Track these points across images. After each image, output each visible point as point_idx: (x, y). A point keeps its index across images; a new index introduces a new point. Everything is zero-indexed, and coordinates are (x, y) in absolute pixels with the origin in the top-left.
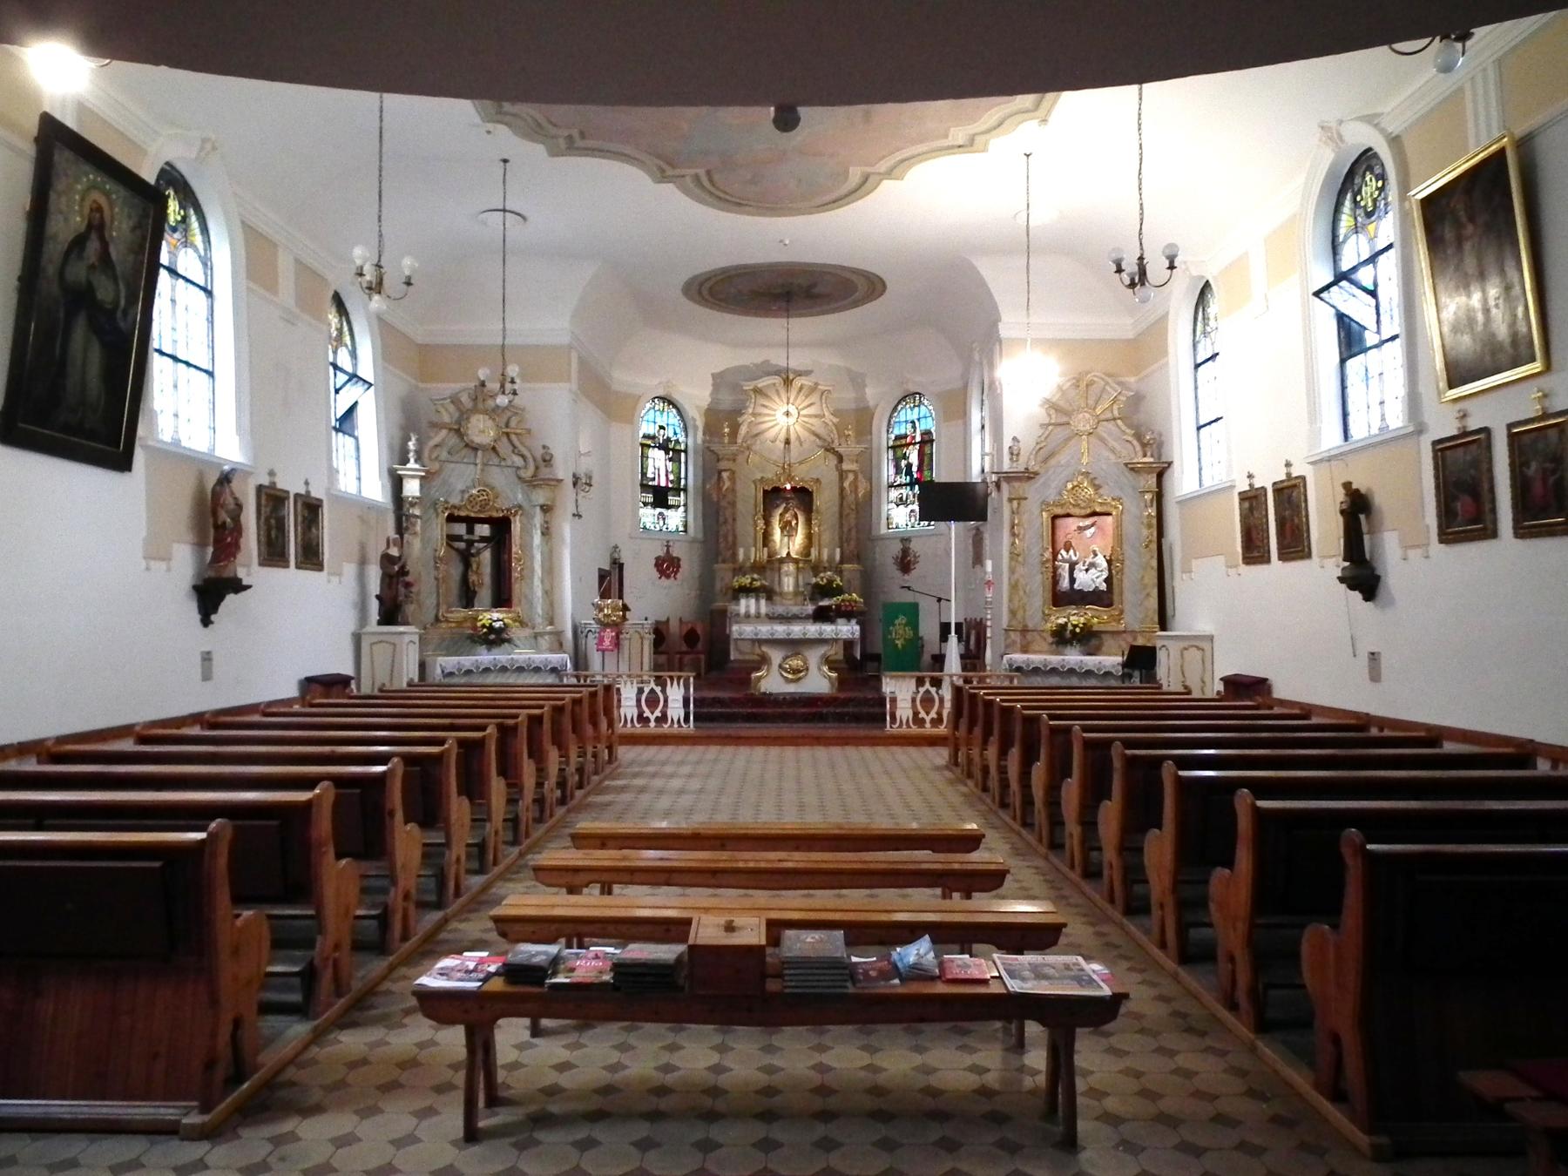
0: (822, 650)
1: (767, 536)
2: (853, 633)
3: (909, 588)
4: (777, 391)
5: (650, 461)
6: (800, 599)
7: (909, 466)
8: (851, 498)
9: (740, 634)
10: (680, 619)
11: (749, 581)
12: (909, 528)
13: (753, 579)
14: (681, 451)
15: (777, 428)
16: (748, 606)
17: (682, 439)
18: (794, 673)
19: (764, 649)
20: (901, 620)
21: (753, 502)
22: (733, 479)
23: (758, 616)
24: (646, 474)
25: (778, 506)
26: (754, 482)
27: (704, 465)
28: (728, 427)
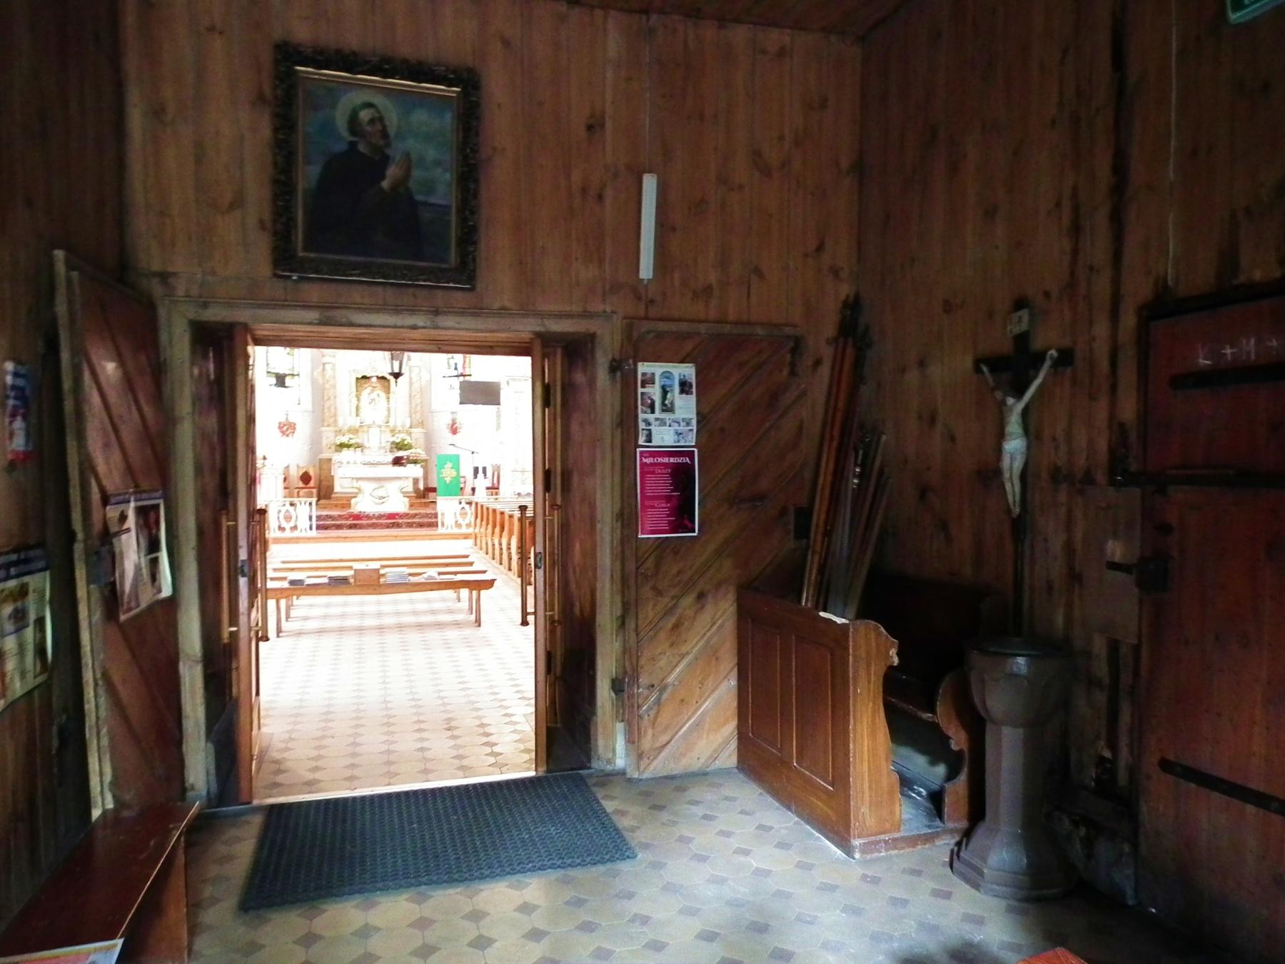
3: (453, 445)
6: (383, 451)
8: (416, 385)
10: (298, 466)
11: (348, 439)
20: (449, 465)
22: (333, 369)
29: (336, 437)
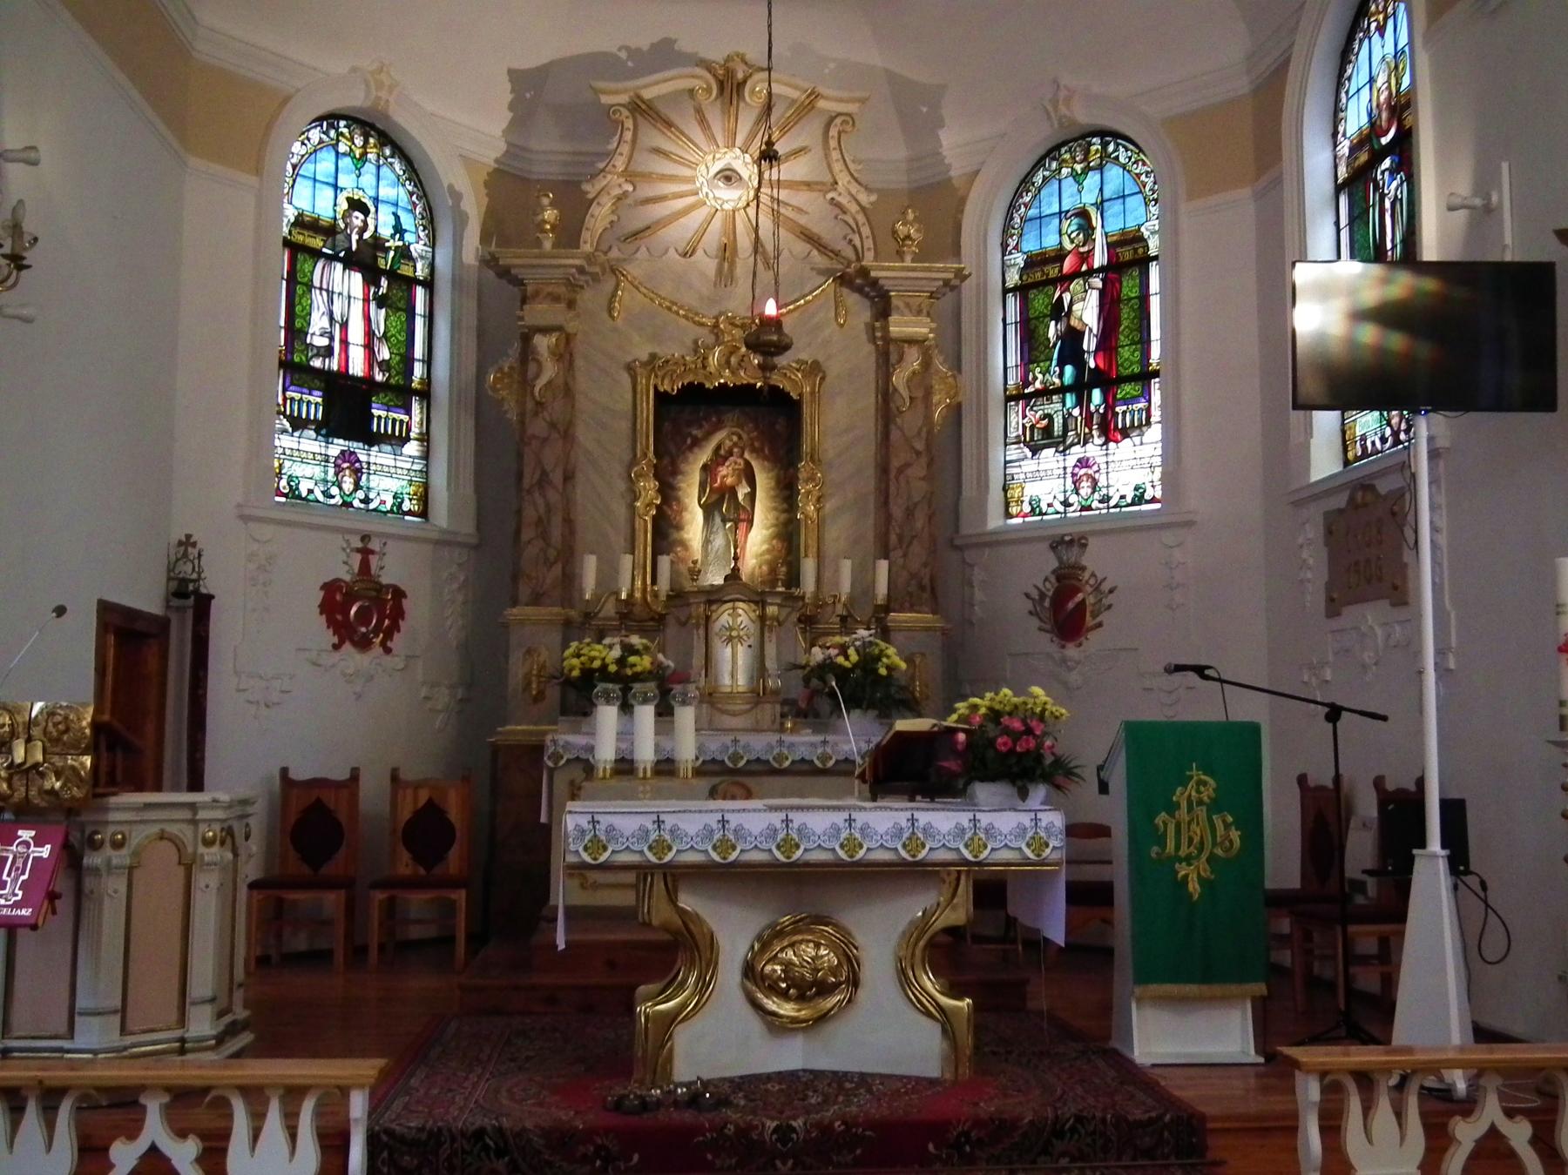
0: (913, 906)
1: (665, 530)
2: (1039, 844)
3: (1200, 671)
4: (699, 111)
5: (319, 299)
6: (769, 711)
7: (1072, 338)
8: (909, 421)
9: (597, 845)
10: (395, 777)
11: (616, 652)
12: (1073, 513)
13: (629, 650)
14: (415, 281)
15: (699, 216)
16: (625, 735)
17: (417, 249)
18: (801, 998)
19: (687, 901)
20: (1199, 787)
21: (624, 426)
22: (565, 355)
23: (666, 767)
24: (303, 333)
25: (697, 443)
26: (630, 368)
27: (481, 321)
28: (553, 204)
29: (565, 646)
